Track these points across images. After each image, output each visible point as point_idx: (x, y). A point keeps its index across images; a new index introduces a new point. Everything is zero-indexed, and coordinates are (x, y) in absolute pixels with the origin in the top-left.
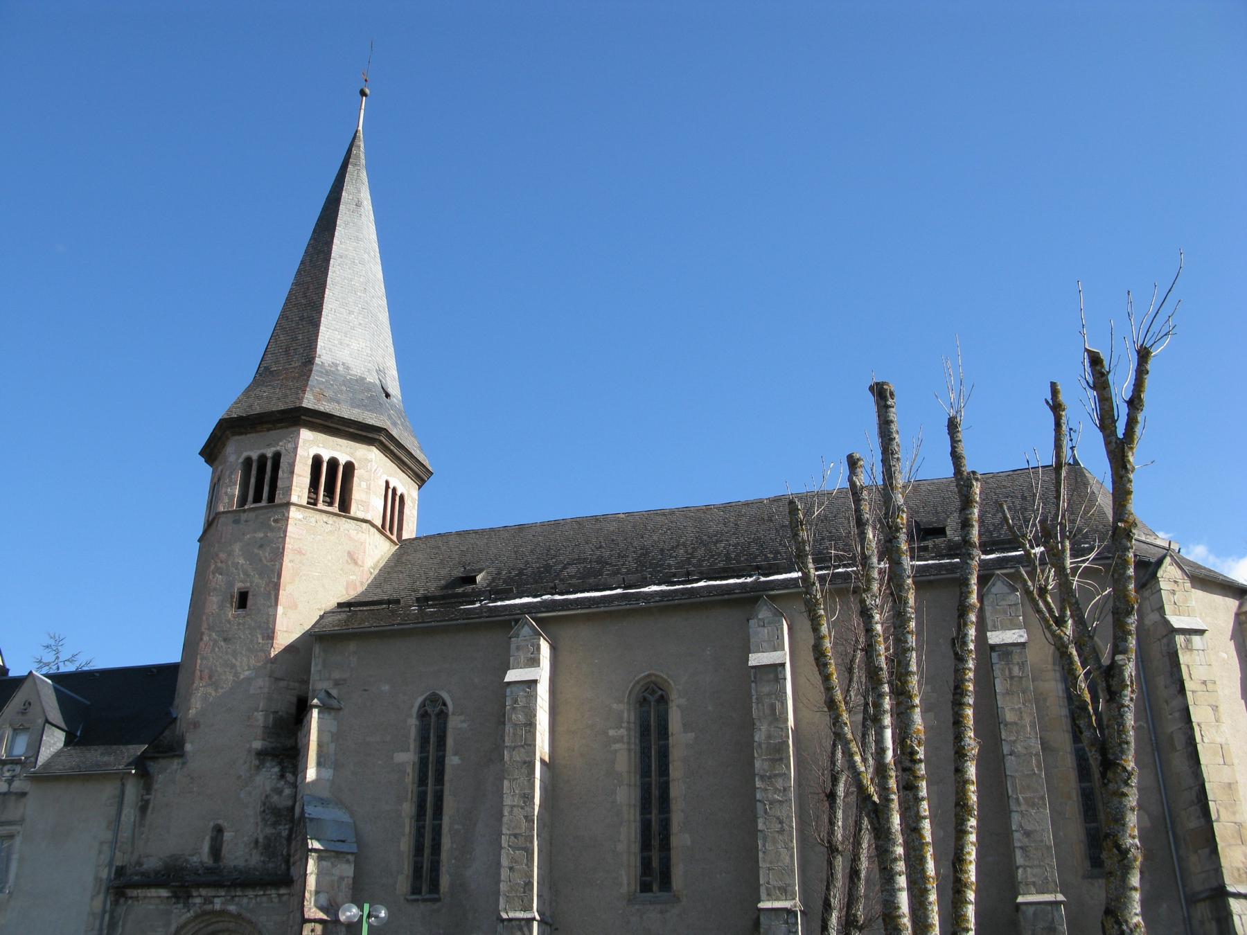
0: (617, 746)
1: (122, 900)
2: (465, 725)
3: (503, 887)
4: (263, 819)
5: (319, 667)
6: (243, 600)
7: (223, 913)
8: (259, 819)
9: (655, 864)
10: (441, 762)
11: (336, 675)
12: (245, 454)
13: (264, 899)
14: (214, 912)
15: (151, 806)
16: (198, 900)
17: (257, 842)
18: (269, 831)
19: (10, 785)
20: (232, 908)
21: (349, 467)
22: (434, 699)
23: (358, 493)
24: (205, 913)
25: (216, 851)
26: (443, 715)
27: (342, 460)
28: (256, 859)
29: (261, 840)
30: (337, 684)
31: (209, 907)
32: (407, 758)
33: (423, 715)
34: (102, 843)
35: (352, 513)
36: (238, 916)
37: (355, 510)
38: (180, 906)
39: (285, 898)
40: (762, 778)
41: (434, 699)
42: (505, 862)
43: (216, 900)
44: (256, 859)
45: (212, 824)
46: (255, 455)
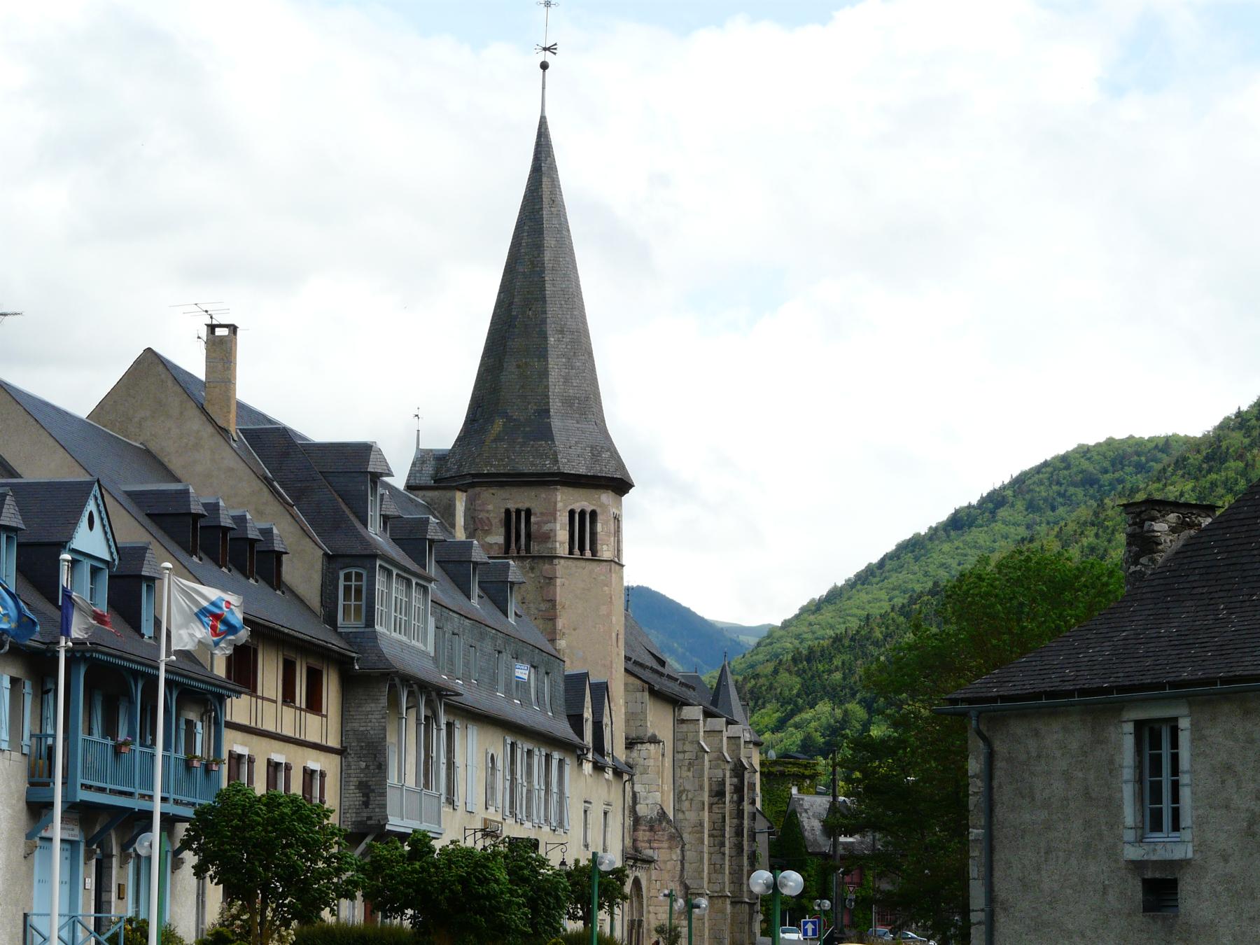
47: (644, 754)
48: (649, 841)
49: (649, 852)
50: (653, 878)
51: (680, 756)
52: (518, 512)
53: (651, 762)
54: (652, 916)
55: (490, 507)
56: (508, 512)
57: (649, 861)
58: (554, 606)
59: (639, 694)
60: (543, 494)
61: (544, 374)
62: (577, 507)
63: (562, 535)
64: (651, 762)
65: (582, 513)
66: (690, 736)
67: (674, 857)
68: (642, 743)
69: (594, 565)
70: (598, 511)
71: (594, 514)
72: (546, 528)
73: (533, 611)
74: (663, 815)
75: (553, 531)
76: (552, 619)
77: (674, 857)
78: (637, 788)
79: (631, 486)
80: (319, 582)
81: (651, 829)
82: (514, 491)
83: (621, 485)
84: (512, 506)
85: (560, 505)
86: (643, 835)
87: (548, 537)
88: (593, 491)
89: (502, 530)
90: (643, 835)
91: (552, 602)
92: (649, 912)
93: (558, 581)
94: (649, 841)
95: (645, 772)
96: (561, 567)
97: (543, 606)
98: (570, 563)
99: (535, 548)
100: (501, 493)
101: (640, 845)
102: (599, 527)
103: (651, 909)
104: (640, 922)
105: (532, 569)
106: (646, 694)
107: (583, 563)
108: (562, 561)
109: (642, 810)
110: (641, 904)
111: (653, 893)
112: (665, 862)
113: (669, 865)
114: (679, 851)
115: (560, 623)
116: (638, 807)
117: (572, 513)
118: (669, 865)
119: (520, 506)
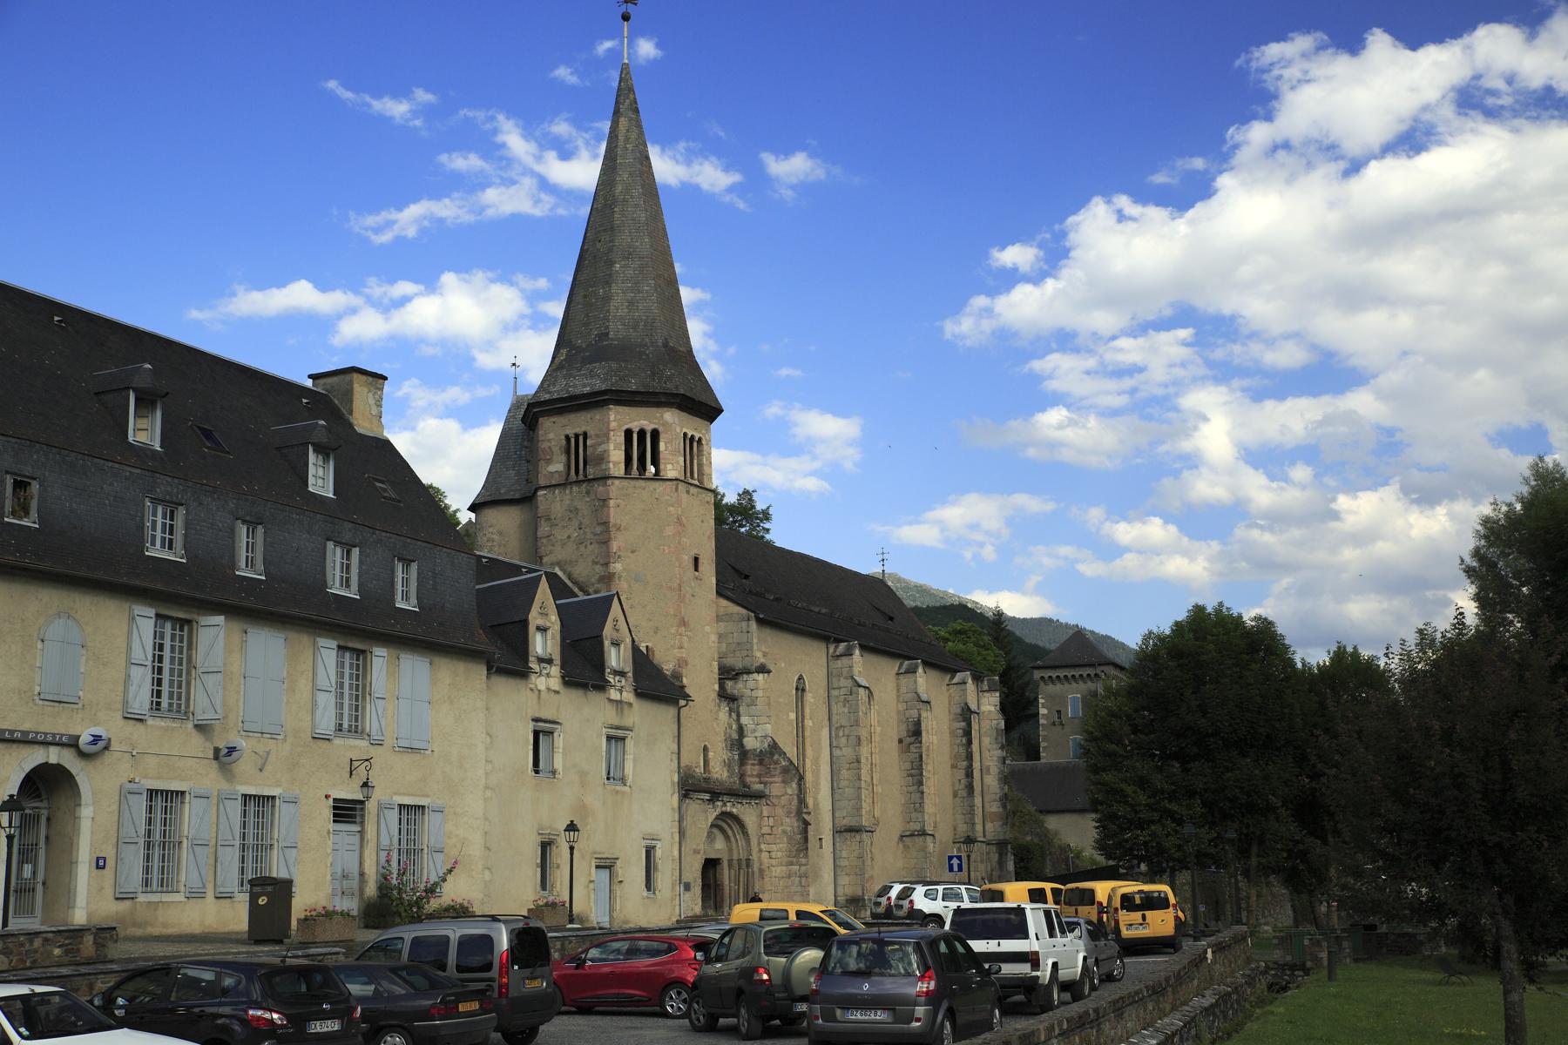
32: (793, 716)
47: (751, 684)
48: (759, 776)
51: (835, 693)
52: (577, 436)
53: (760, 693)
54: (765, 855)
55: (551, 436)
56: (568, 438)
57: (759, 796)
58: (608, 531)
59: (744, 624)
60: (597, 415)
61: (607, 299)
62: (635, 426)
63: (617, 455)
64: (760, 693)
65: (642, 433)
66: (845, 671)
67: (789, 791)
68: (749, 672)
69: (656, 484)
70: (661, 429)
71: (655, 434)
72: (600, 449)
73: (589, 536)
74: (774, 747)
75: (606, 451)
76: (605, 542)
77: (789, 791)
78: (744, 720)
79: (719, 411)
80: (714, 581)
81: (761, 763)
82: (572, 416)
83: (708, 410)
84: (570, 432)
85: (613, 425)
86: (752, 769)
87: (602, 458)
88: (654, 410)
89: (563, 458)
90: (752, 769)
91: (606, 523)
93: (612, 503)
94: (759, 776)
95: (753, 702)
96: (615, 487)
97: (598, 529)
98: (625, 483)
99: (590, 470)
100: (561, 420)
101: (748, 779)
102: (662, 446)
104: (748, 860)
105: (588, 493)
106: (753, 625)
107: (642, 483)
108: (617, 482)
109: (750, 743)
110: (748, 841)
111: (766, 830)
112: (778, 797)
113: (784, 800)
114: (794, 785)
115: (614, 546)
116: (746, 741)
117: (628, 433)
118: (784, 800)
119: (578, 430)
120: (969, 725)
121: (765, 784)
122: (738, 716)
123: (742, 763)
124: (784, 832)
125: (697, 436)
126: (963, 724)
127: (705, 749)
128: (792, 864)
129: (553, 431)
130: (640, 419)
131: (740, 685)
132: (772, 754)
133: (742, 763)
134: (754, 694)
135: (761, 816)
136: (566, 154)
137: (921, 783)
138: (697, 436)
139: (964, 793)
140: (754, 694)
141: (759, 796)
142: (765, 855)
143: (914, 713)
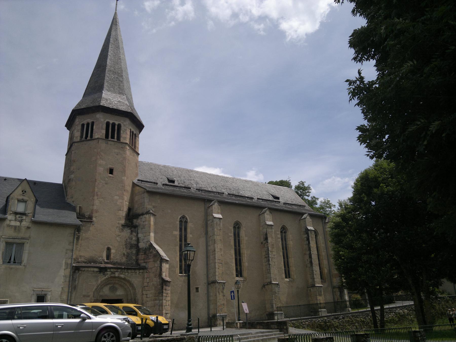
0: (231, 238)
1: (77, 271)
2: (193, 226)
3: (217, 274)
4: (126, 247)
5: (148, 201)
6: (111, 171)
7: (118, 277)
8: (124, 247)
9: (239, 269)
10: (186, 236)
11: (153, 204)
12: (107, 120)
13: (134, 273)
14: (115, 277)
15: (80, 238)
16: (109, 273)
17: (124, 254)
18: (129, 251)
19: (21, 223)
20: (122, 276)
21: (119, 126)
22: (183, 217)
23: (123, 135)
24: (111, 277)
25: (108, 257)
26: (186, 222)
27: (117, 123)
28: (124, 260)
29: (126, 254)
30: (154, 207)
31: (113, 275)
32: (177, 233)
33: (181, 221)
34: (67, 250)
35: (121, 141)
36: (124, 279)
37: (122, 140)
38: (102, 274)
39: (141, 273)
40: (271, 251)
41: (183, 217)
42: (217, 267)
43: (116, 273)
44: (124, 260)
45: (106, 247)
46: (111, 122)
47: (143, 219)
49: (144, 264)
50: (146, 277)
57: (144, 268)
67: (156, 265)
70: (95, 121)
71: (93, 123)
77: (156, 265)
81: (145, 253)
86: (141, 257)
92: (143, 294)
94: (144, 259)
101: (140, 262)
102: (94, 127)
103: (144, 292)
111: (146, 284)
112: (151, 268)
114: (158, 262)
117: (108, 124)
120: (308, 235)
121: (146, 263)
122: (138, 234)
123: (137, 254)
124: (153, 284)
125: (117, 123)
126: (306, 235)
127: (109, 249)
128: (156, 300)
129: (79, 121)
130: (116, 120)
131: (139, 221)
132: (150, 249)
133: (137, 254)
134: (144, 223)
135: (143, 278)
136: (386, 28)
137: (269, 261)
138: (135, 132)
139: (309, 265)
140: (144, 223)
141: (144, 268)
142: (145, 296)
143: (265, 230)
